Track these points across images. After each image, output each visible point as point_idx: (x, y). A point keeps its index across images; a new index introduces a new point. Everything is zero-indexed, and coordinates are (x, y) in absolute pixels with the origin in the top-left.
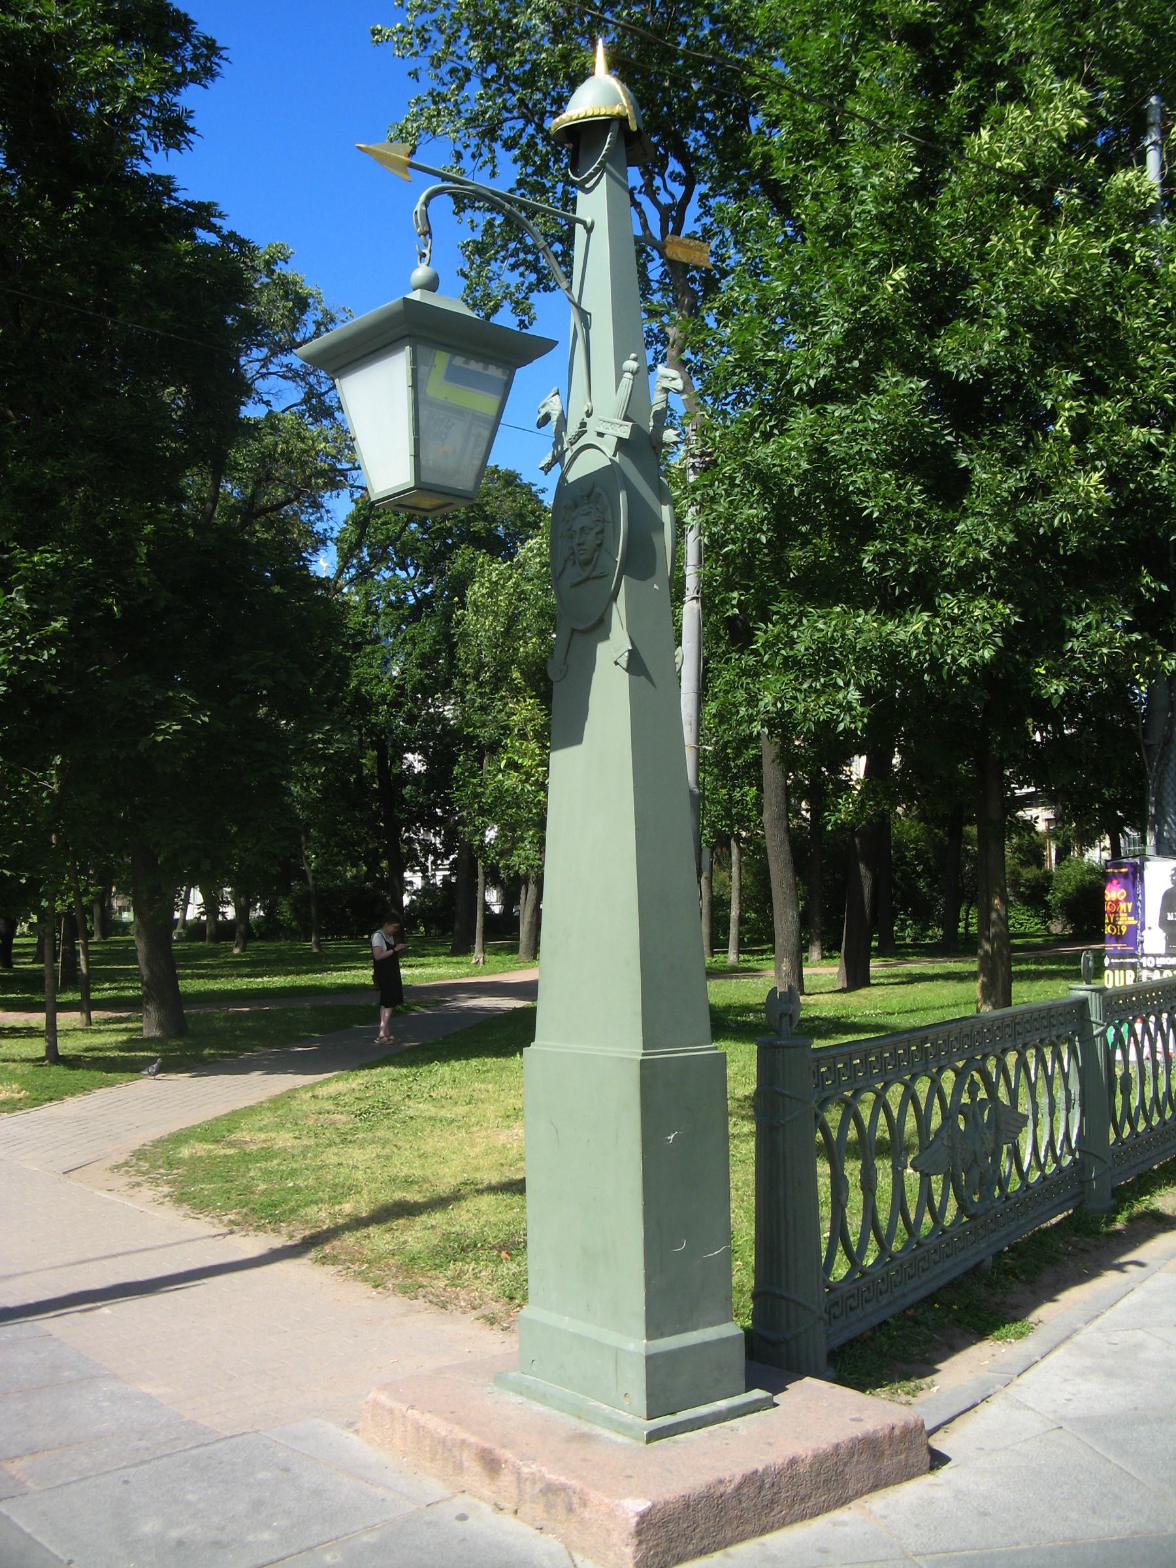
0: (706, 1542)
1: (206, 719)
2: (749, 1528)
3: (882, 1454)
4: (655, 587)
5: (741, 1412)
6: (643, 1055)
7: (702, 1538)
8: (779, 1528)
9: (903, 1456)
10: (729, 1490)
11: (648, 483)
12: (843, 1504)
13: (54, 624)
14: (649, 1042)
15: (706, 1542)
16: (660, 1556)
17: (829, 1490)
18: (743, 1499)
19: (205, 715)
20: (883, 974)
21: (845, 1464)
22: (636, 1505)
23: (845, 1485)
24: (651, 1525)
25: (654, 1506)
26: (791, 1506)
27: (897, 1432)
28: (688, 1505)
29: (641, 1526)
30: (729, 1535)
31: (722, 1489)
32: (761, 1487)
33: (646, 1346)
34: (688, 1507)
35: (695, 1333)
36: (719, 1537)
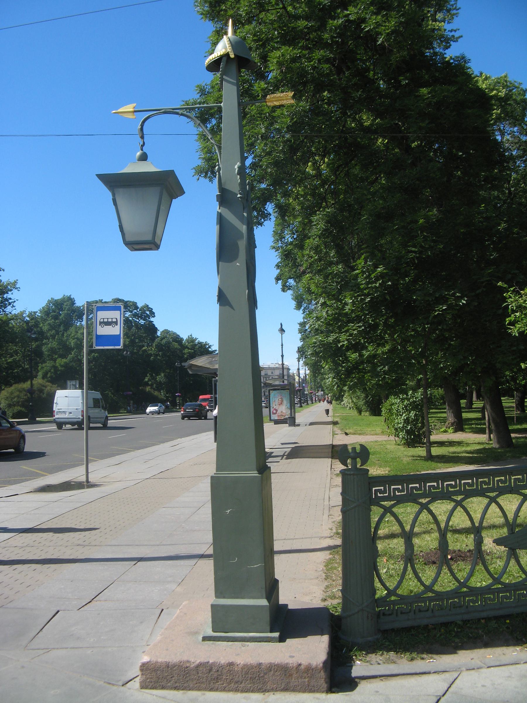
0: (177, 684)
1: (465, 302)
2: (204, 686)
3: (291, 675)
4: (238, 264)
5: (258, 640)
6: (215, 474)
7: (176, 682)
8: (221, 691)
9: (307, 680)
10: (192, 666)
11: (237, 218)
12: (263, 692)
13: (379, 269)
14: (218, 469)
15: (177, 684)
16: (153, 683)
17: (254, 683)
18: (200, 672)
19: (464, 300)
20: (477, 441)
21: (265, 674)
22: (146, 659)
23: (265, 683)
24: (147, 669)
25: (150, 661)
26: (230, 683)
27: (302, 667)
28: (168, 667)
29: (142, 668)
30: (191, 686)
31: (188, 665)
32: (210, 670)
33: (214, 600)
34: (168, 667)
35: (242, 600)
36: (186, 685)
